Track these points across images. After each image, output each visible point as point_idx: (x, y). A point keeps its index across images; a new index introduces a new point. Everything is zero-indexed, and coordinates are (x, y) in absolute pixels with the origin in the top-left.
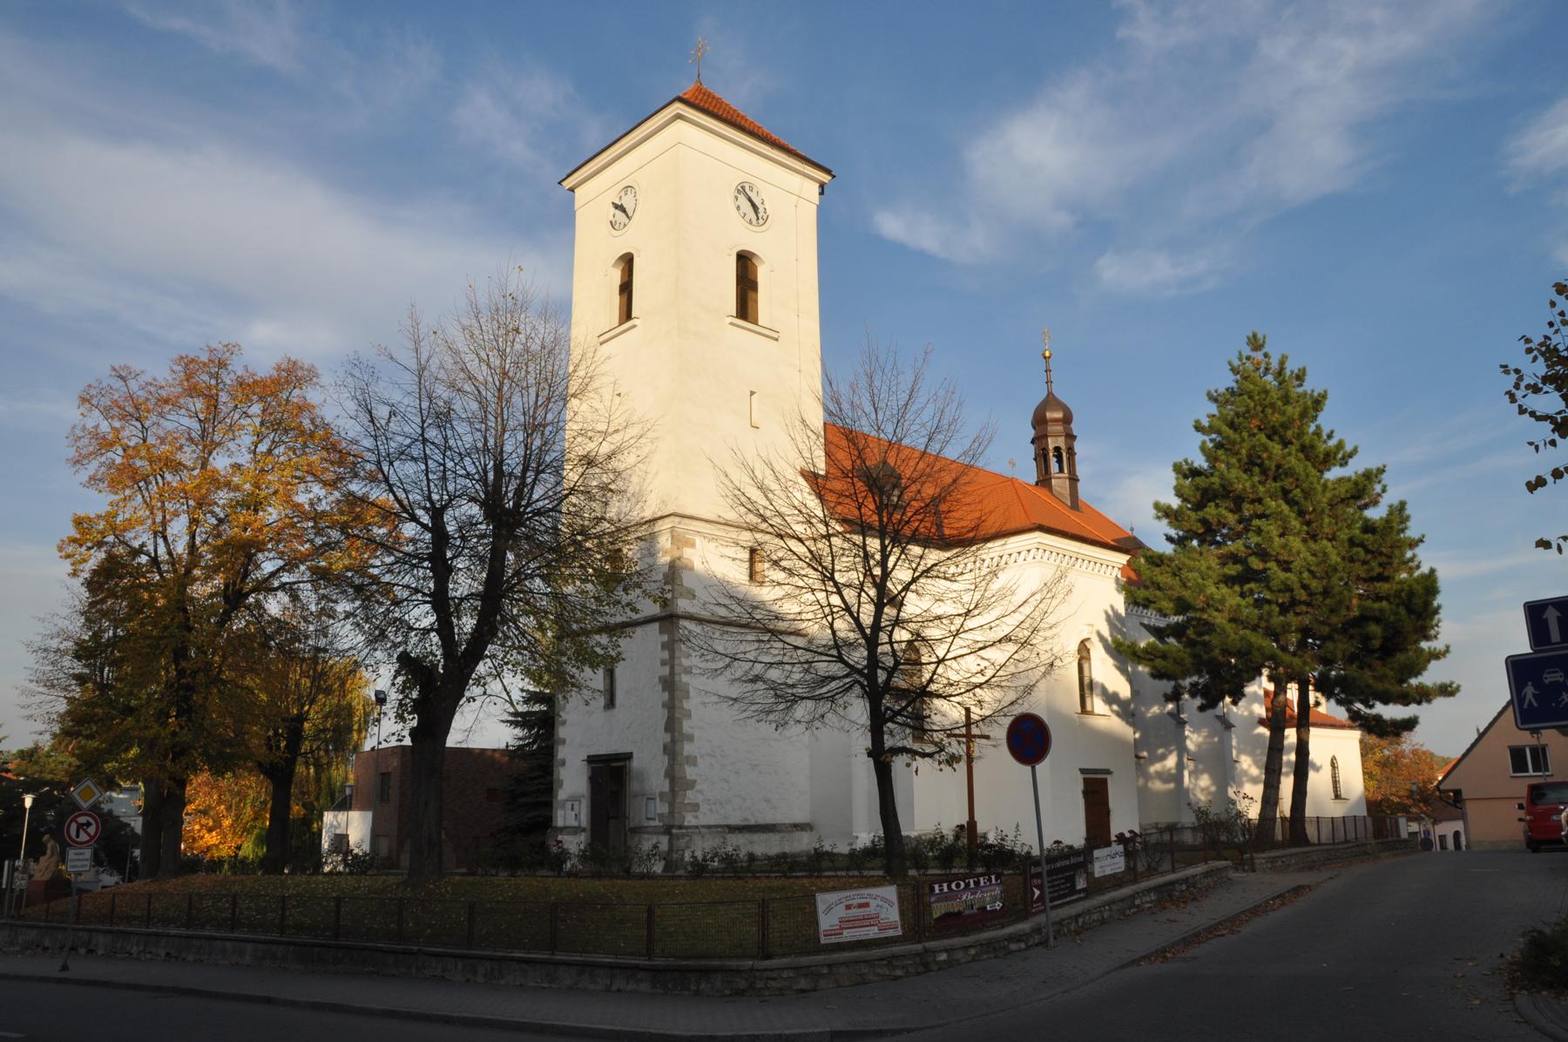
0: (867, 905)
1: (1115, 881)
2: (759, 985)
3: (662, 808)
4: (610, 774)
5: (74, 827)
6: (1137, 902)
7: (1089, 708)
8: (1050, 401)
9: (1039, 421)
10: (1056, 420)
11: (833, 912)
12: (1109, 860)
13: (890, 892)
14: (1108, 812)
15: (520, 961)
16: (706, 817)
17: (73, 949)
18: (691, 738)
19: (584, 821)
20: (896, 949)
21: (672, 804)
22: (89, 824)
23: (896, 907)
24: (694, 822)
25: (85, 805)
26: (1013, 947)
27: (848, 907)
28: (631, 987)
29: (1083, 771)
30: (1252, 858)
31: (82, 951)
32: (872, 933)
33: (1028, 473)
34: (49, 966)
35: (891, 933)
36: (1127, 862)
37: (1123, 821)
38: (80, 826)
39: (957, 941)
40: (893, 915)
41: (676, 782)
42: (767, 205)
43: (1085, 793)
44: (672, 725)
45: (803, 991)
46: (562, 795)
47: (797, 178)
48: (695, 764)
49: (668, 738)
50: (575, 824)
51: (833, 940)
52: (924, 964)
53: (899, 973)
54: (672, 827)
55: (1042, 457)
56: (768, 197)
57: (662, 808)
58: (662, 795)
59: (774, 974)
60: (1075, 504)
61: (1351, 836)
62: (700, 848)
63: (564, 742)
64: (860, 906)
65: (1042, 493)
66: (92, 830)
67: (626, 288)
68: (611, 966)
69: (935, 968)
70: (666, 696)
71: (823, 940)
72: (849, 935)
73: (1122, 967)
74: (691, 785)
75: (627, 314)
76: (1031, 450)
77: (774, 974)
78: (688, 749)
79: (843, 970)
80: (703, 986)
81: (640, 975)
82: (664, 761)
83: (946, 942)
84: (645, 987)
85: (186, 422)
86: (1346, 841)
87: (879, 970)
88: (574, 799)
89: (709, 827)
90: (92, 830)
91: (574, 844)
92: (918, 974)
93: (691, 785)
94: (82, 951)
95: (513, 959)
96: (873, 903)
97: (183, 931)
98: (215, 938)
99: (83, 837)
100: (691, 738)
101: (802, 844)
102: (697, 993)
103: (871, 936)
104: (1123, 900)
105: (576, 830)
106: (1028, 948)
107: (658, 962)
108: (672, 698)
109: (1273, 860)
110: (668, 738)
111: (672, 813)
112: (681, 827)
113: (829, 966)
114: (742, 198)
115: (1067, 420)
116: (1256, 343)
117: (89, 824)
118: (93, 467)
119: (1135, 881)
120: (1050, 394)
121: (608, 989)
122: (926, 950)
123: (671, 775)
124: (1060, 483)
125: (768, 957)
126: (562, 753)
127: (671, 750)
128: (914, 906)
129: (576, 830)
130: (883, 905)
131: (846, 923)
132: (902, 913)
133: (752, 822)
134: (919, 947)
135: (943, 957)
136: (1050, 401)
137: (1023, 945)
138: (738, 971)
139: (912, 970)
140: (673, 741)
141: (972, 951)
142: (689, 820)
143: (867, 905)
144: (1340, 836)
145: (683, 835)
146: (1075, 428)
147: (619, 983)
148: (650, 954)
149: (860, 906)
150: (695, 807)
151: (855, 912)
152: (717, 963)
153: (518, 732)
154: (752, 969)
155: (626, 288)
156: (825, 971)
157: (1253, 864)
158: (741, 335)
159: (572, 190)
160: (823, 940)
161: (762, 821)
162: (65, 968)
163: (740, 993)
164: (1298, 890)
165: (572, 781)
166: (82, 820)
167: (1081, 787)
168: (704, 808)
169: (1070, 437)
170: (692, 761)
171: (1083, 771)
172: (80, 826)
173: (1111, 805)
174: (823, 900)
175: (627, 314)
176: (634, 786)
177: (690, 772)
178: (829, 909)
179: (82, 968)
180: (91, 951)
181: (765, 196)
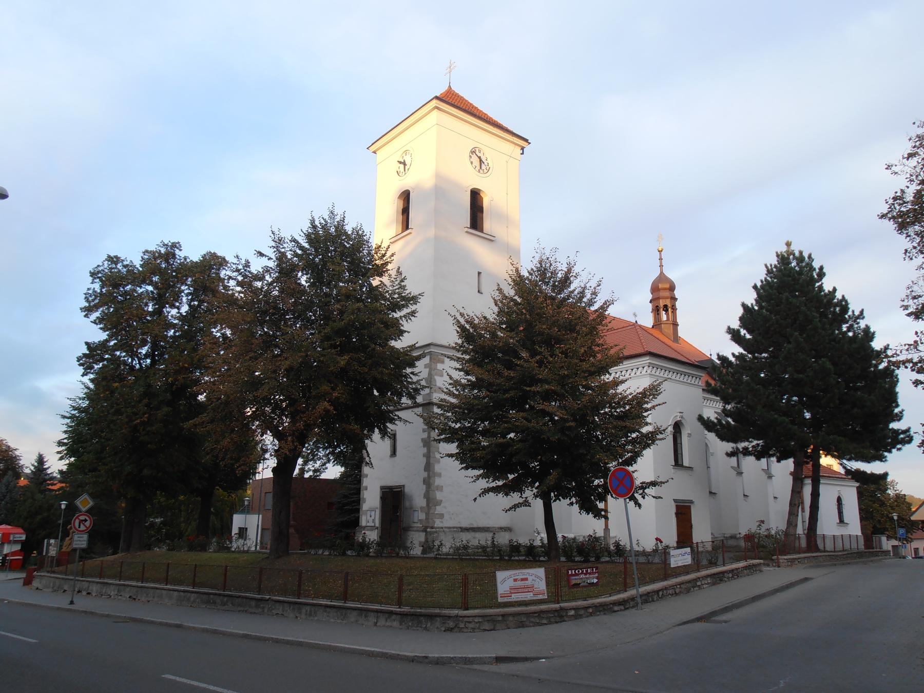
0: (526, 579)
1: (685, 570)
2: (462, 625)
3: (422, 516)
4: (393, 498)
5: (77, 522)
6: (699, 583)
7: (680, 463)
8: (662, 278)
9: (655, 289)
10: (665, 289)
11: (506, 581)
12: (681, 557)
13: (541, 572)
14: (691, 527)
15: (327, 606)
16: (448, 522)
17: (79, 592)
18: (440, 475)
19: (377, 524)
20: (544, 607)
21: (427, 514)
22: (86, 520)
23: (544, 582)
24: (440, 525)
25: (84, 510)
26: (616, 608)
27: (515, 580)
28: (388, 624)
29: (675, 501)
30: (778, 559)
31: (84, 593)
32: (529, 596)
33: (647, 320)
34: (61, 601)
35: (541, 597)
36: (693, 559)
37: (702, 533)
38: (81, 521)
39: (580, 603)
40: (542, 585)
41: (431, 501)
42: (489, 161)
43: (677, 514)
44: (428, 467)
45: (485, 630)
46: (365, 507)
47: (467, 126)
48: (442, 490)
49: (425, 474)
50: (371, 524)
51: (506, 600)
52: (559, 616)
53: (545, 621)
54: (426, 527)
55: (656, 310)
56: (489, 156)
57: (422, 516)
58: (421, 508)
59: (470, 619)
60: (676, 338)
61: (847, 546)
62: (447, 544)
63: (367, 476)
64: (522, 580)
65: (656, 333)
66: (87, 524)
67: (406, 211)
68: (377, 611)
69: (566, 619)
70: (425, 450)
71: (500, 600)
72: (515, 597)
73: (685, 623)
74: (439, 503)
75: (406, 225)
76: (650, 306)
77: (470, 619)
78: (438, 481)
79: (511, 618)
80: (429, 625)
81: (394, 617)
82: (423, 488)
83: (574, 604)
84: (396, 624)
85: (150, 288)
86: (843, 550)
87: (532, 620)
88: (372, 510)
89: (449, 528)
90: (87, 524)
91: (373, 536)
92: (556, 622)
93: (439, 503)
94: (84, 593)
95: (321, 605)
96: (530, 578)
97: (140, 584)
98: (157, 588)
99: (83, 528)
100: (440, 475)
101: (503, 539)
102: (426, 629)
103: (529, 598)
104: (689, 582)
105: (373, 528)
106: (626, 609)
107: (406, 609)
108: (429, 451)
109: (792, 561)
110: (425, 474)
111: (427, 519)
112: (432, 528)
113: (503, 616)
114: (474, 156)
115: (672, 288)
116: (788, 244)
117: (86, 520)
118: (96, 315)
119: (698, 570)
120: (662, 272)
121: (376, 624)
122: (562, 609)
123: (428, 496)
124: (668, 329)
125: (467, 609)
126: (365, 482)
127: (428, 482)
128: (553, 580)
129: (373, 528)
130: (536, 579)
131: (514, 590)
132: (547, 585)
133: (475, 526)
134: (557, 606)
135: (572, 613)
136: (662, 278)
137: (622, 608)
138: (449, 617)
139: (553, 620)
140: (429, 476)
141: (591, 610)
142: (438, 523)
143: (526, 579)
144: (839, 546)
145: (434, 533)
146: (677, 293)
147: (382, 622)
148: (400, 604)
149: (522, 580)
150: (441, 516)
151: (519, 583)
152: (437, 611)
153: (738, 350)
154: (457, 616)
155: (406, 211)
156: (500, 618)
157: (778, 562)
158: (473, 245)
159: (375, 152)
160: (500, 600)
161: (481, 525)
162: (72, 603)
163: (450, 630)
164: (806, 580)
165: (371, 500)
166: (82, 518)
167: (674, 510)
168: (446, 517)
169: (674, 299)
170: (440, 488)
171: (675, 501)
172: (81, 521)
173: (693, 522)
174: (501, 575)
175: (406, 225)
176: (407, 504)
177: (439, 495)
178: (504, 581)
179: (82, 603)
180: (89, 593)
181: (487, 155)
